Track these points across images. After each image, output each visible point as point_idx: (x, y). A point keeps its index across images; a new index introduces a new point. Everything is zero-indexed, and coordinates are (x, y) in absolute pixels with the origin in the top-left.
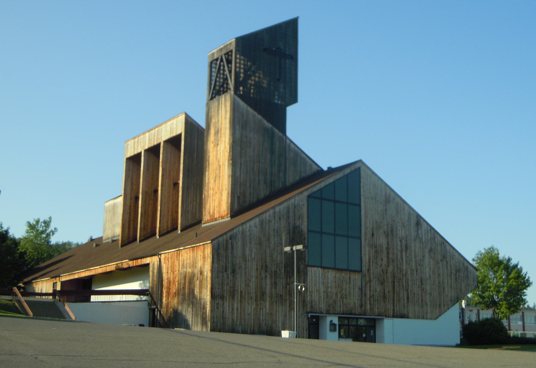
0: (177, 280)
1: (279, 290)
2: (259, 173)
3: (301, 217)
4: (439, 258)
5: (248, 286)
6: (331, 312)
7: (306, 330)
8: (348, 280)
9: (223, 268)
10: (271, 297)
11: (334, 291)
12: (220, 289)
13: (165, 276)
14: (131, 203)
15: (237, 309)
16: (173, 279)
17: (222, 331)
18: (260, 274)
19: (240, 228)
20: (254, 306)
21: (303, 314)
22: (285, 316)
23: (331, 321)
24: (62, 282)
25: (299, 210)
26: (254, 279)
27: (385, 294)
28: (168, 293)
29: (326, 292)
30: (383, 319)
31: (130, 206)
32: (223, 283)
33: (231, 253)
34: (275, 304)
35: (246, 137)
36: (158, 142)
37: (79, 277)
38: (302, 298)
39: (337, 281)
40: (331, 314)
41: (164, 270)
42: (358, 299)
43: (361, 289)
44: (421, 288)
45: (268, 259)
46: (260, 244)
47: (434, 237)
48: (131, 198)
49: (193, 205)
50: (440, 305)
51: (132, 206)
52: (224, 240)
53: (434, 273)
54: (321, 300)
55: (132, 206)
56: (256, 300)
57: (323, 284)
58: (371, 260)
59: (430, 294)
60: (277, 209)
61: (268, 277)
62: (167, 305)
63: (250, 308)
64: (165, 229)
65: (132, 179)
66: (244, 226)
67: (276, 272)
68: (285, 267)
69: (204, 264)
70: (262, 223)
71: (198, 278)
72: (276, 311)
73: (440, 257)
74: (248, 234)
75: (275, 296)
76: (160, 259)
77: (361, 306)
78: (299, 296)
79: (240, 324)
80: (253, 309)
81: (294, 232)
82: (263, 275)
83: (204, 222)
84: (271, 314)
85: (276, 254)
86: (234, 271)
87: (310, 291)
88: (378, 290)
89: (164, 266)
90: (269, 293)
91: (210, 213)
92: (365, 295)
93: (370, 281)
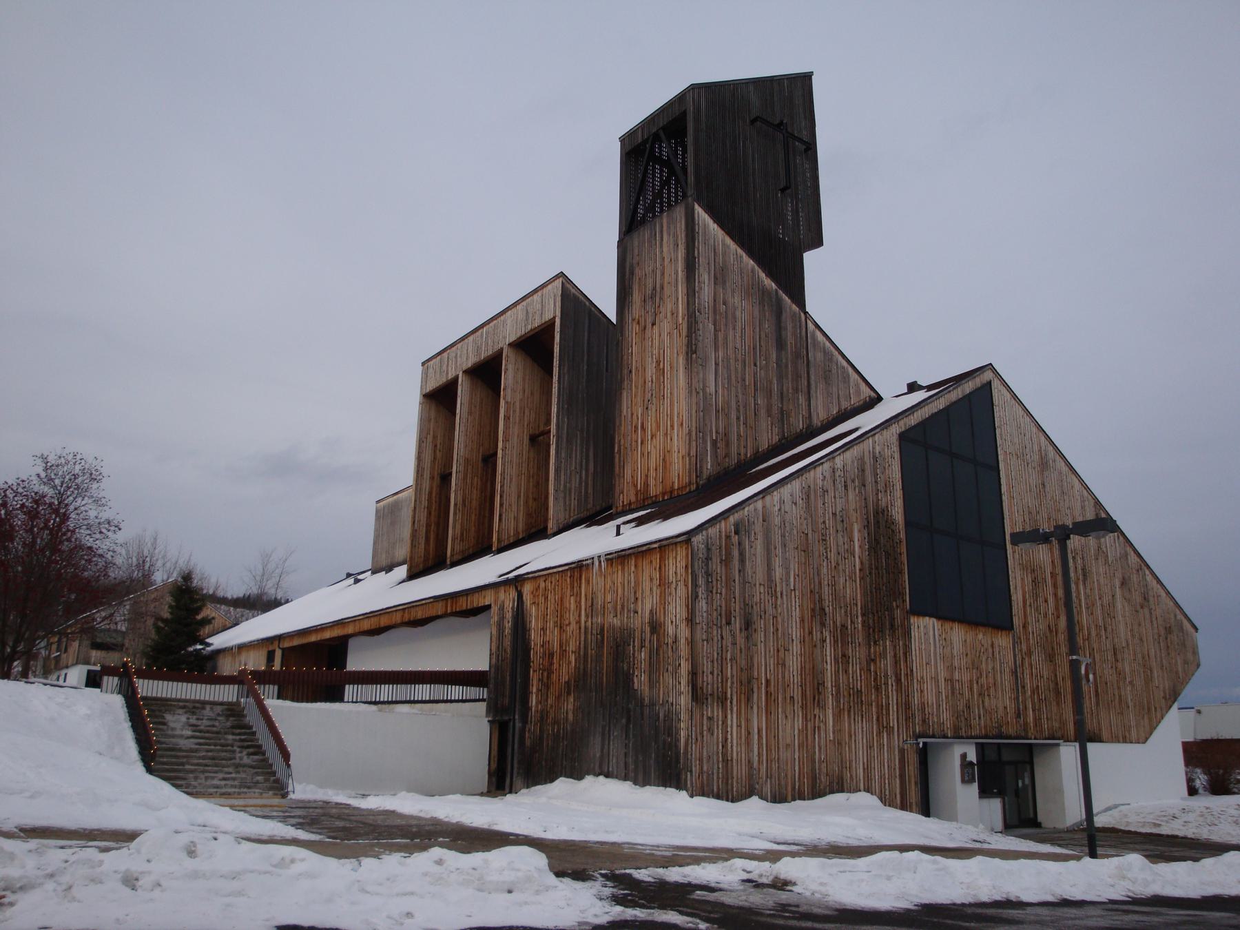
0: (572, 646)
1: (853, 677)
2: (756, 390)
3: (888, 486)
4: (1138, 601)
5: (784, 665)
6: (964, 734)
7: (916, 783)
8: (990, 650)
9: (720, 615)
10: (837, 696)
11: (966, 677)
12: (715, 676)
13: (535, 637)
14: (431, 488)
15: (759, 731)
16: (561, 646)
17: (724, 798)
18: (810, 633)
19: (759, 504)
20: (799, 723)
21: (907, 740)
22: (870, 747)
23: (964, 756)
24: (283, 650)
25: (885, 468)
26: (796, 648)
27: (1057, 684)
28: (546, 685)
29: (950, 681)
30: (1058, 745)
31: (430, 493)
32: (722, 659)
33: (740, 571)
34: (846, 713)
35: (724, 303)
36: (497, 348)
37: (319, 639)
38: (903, 696)
39: (969, 653)
40: (962, 737)
41: (534, 624)
42: (1010, 698)
43: (1014, 672)
44: (1116, 668)
45: (826, 590)
46: (806, 550)
47: (1126, 555)
48: (432, 478)
49: (581, 477)
50: (1149, 709)
51: (434, 495)
52: (720, 536)
53: (1133, 636)
54: (941, 703)
55: (434, 495)
56: (804, 707)
57: (943, 658)
58: (1028, 603)
59: (1131, 683)
60: (839, 461)
61: (828, 641)
62: (543, 716)
63: (791, 727)
64: (512, 534)
65: (435, 437)
66: (768, 498)
67: (844, 626)
68: (863, 615)
69: (663, 602)
70: (807, 493)
71: (642, 641)
72: (850, 736)
73: (1139, 600)
74: (777, 521)
75: (846, 693)
76: (520, 596)
77: (1018, 716)
78: (897, 691)
79: (767, 777)
80: (796, 732)
81: (877, 523)
82: (817, 636)
83: (620, 509)
84: (840, 744)
85: (842, 580)
86: (748, 625)
87: (919, 678)
88: (1045, 674)
89: (533, 612)
90: (832, 685)
91: (636, 486)
92: (1023, 687)
93: (1029, 653)
